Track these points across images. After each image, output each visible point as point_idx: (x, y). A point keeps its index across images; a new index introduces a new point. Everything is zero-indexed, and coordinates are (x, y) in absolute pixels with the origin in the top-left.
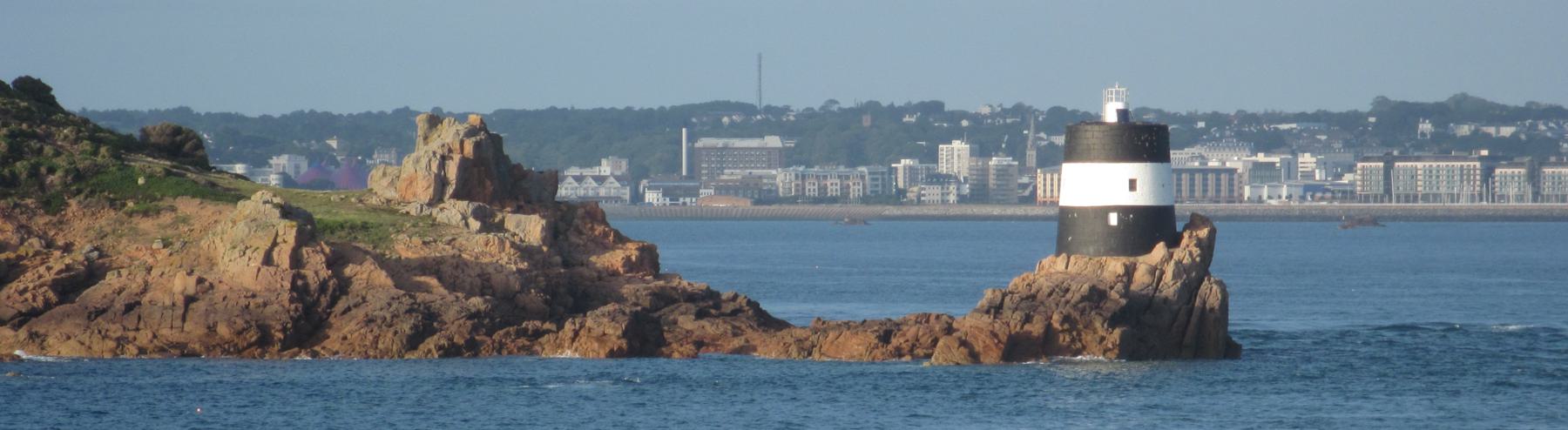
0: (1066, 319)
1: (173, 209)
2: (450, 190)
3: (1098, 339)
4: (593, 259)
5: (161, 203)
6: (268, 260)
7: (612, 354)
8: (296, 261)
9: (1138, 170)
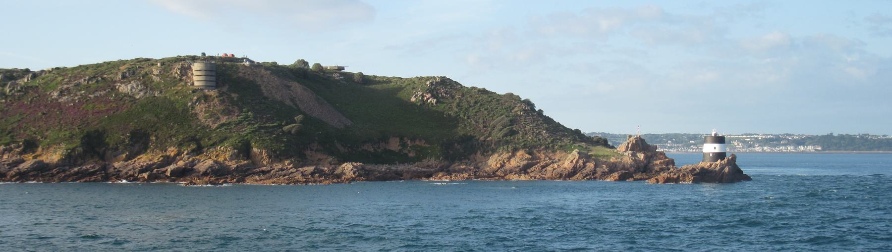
2: (629, 149)
8: (577, 162)
9: (717, 145)
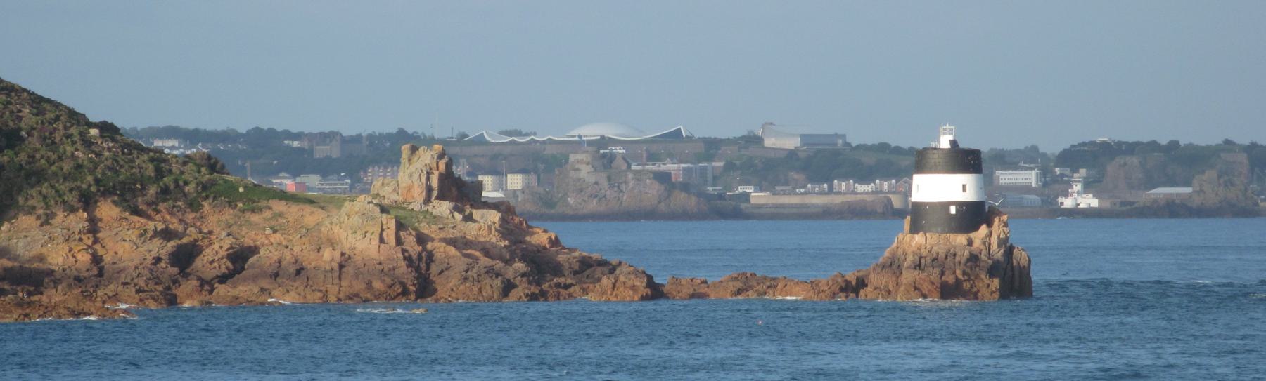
0: (964, 273)
1: (270, 208)
2: (435, 194)
3: (986, 286)
4: (528, 238)
5: (259, 204)
6: (382, 240)
7: (643, 298)
